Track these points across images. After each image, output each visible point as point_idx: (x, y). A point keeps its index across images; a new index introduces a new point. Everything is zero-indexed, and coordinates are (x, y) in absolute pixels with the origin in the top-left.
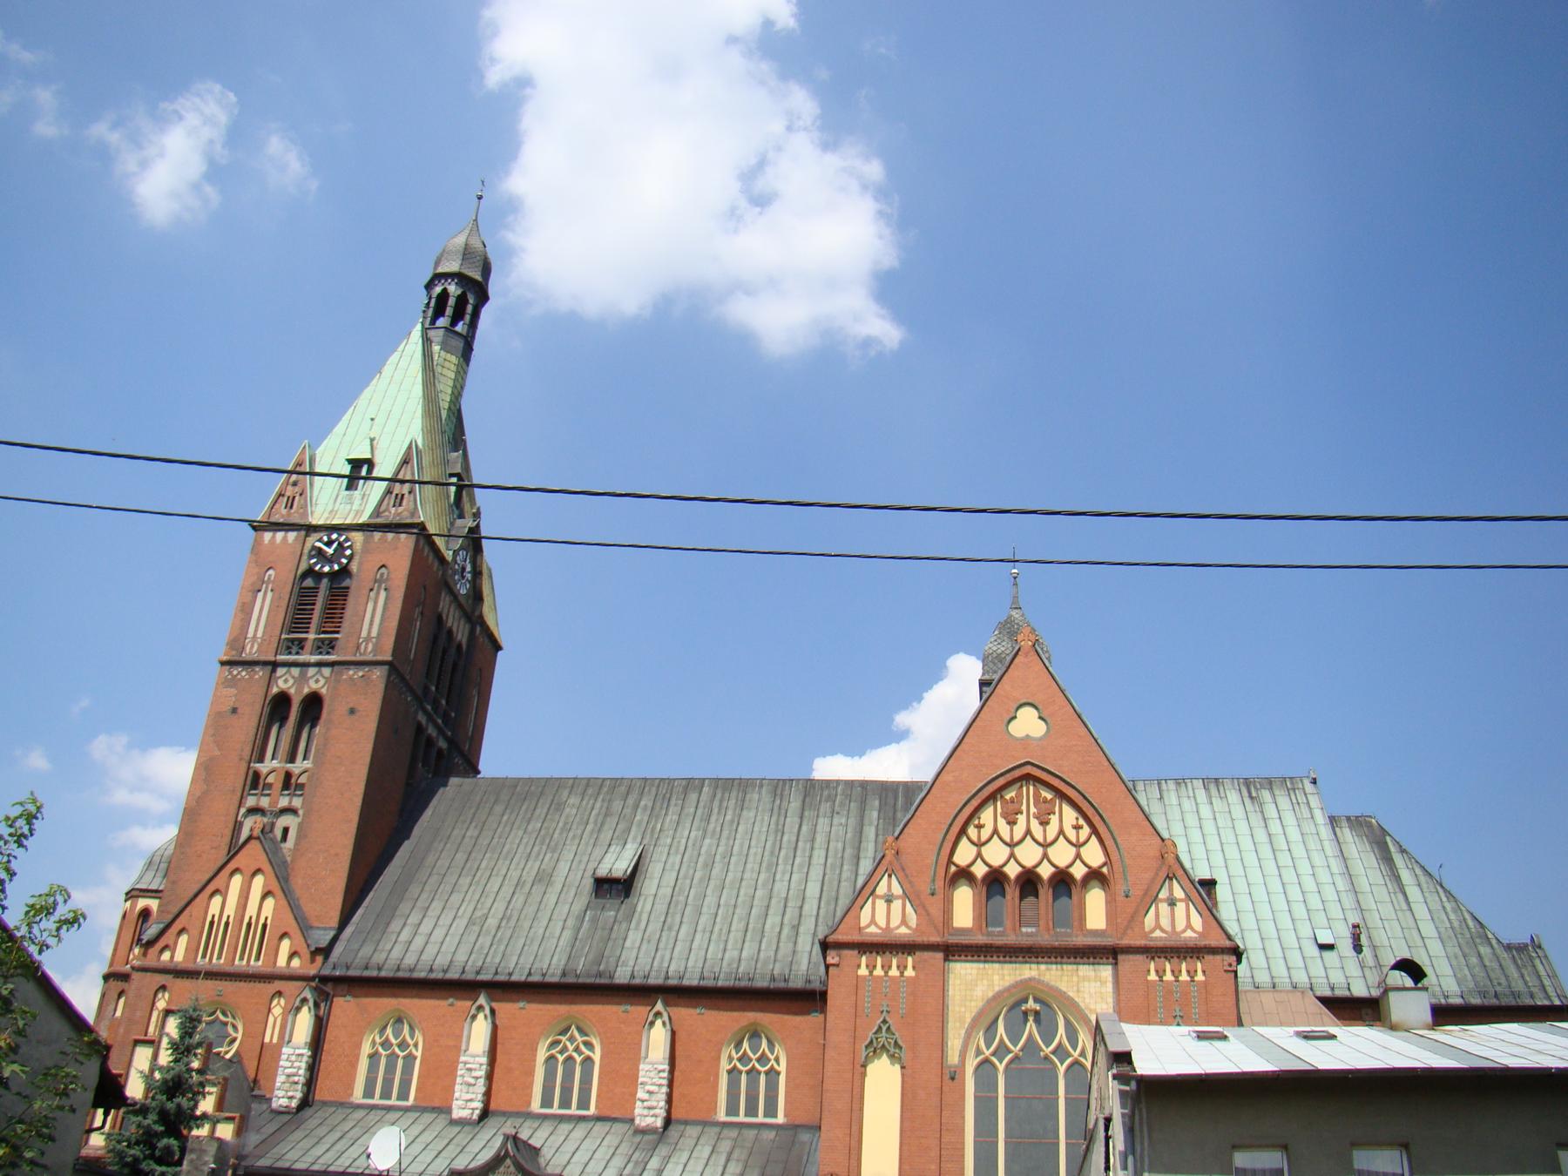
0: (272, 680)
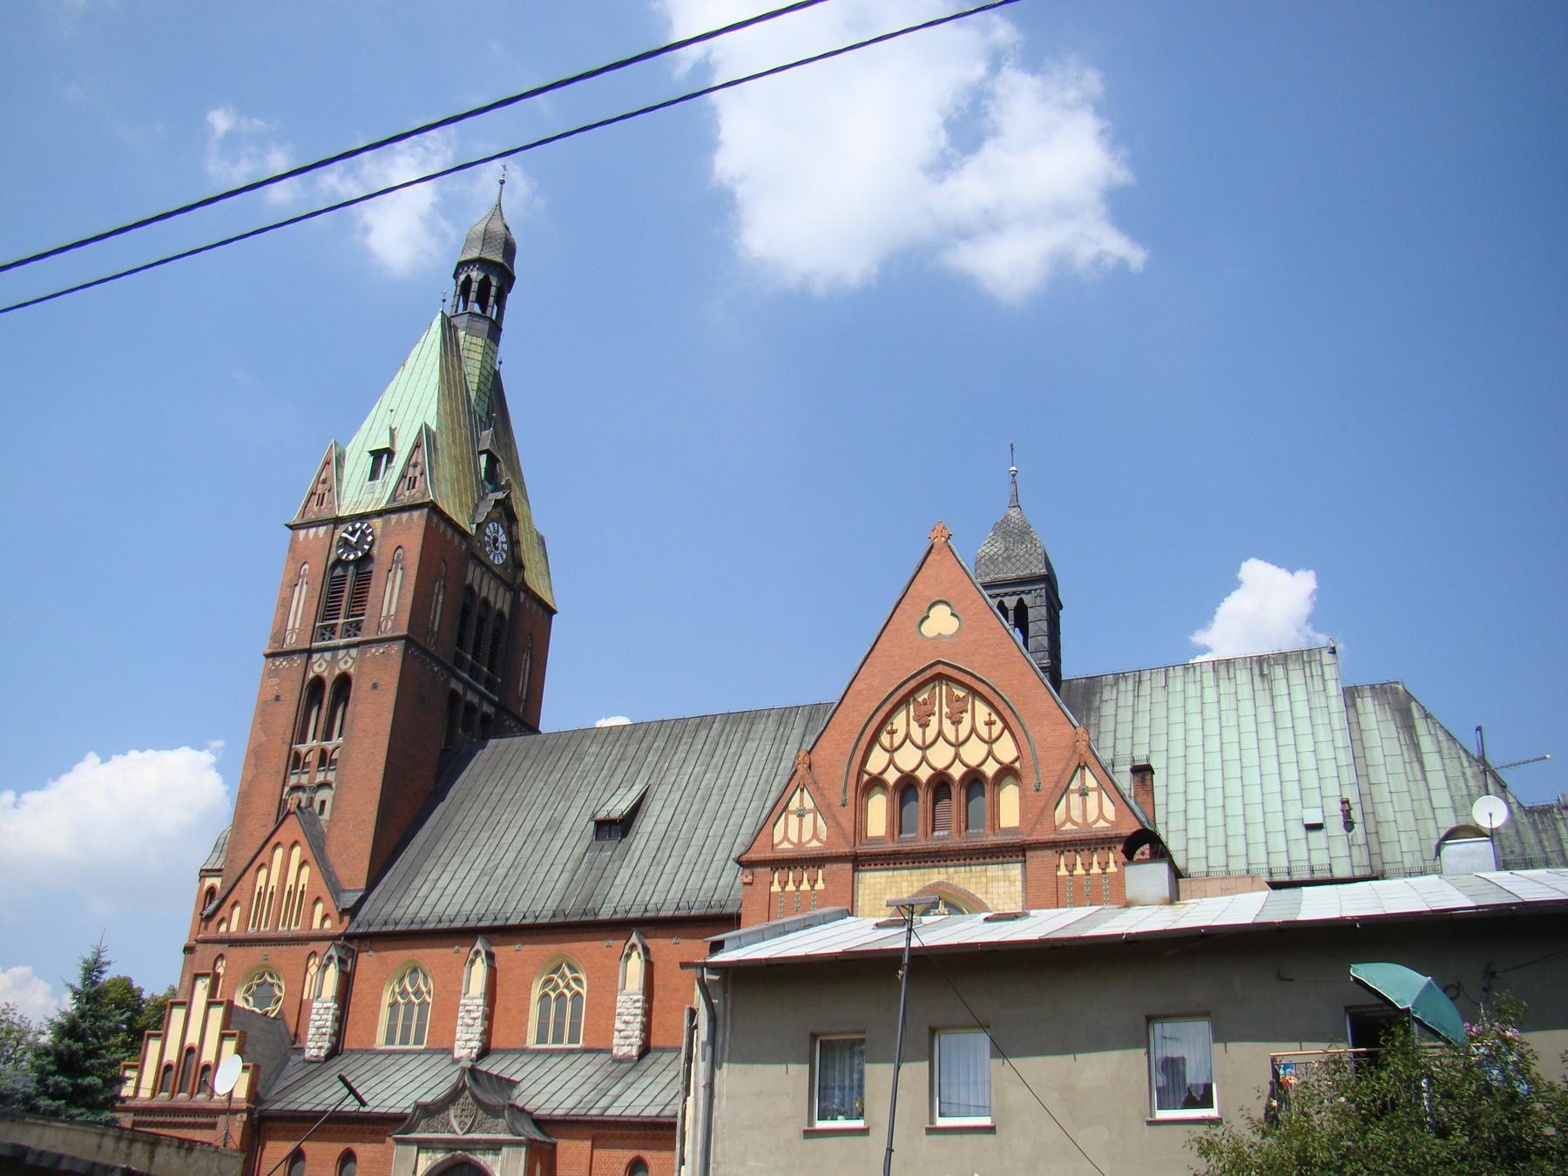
0: (309, 665)
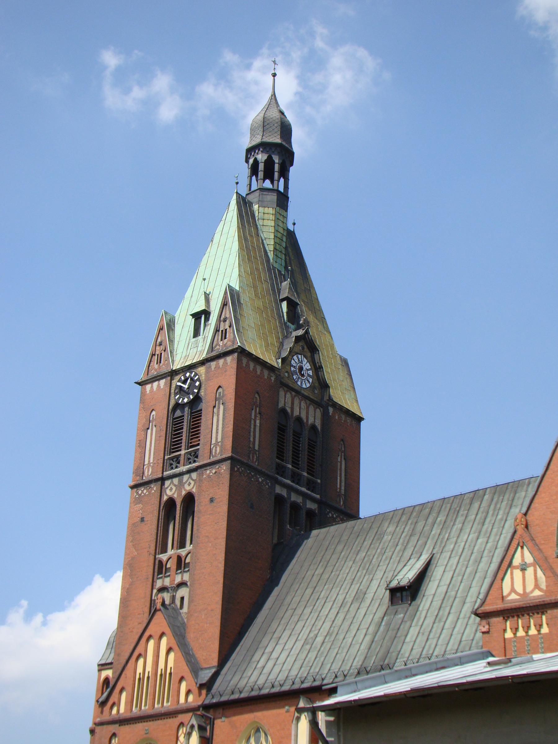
0: (163, 490)
